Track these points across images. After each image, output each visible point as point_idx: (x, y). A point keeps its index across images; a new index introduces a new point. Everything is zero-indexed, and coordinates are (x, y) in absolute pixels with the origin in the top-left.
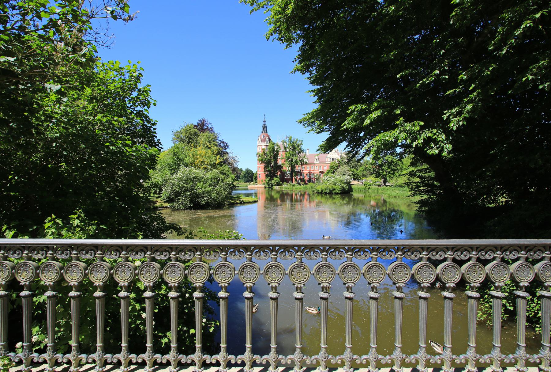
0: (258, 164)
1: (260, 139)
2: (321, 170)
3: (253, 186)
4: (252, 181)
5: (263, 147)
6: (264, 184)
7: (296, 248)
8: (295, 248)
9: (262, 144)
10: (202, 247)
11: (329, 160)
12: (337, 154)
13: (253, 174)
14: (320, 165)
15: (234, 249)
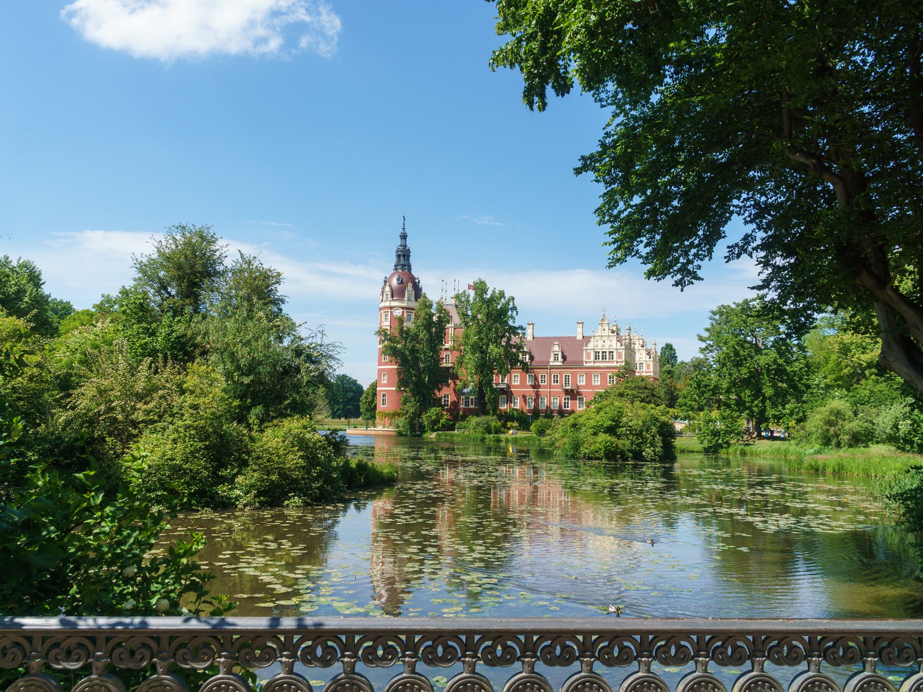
0: (380, 364)
1: (388, 289)
2: (569, 387)
3: (361, 430)
4: (357, 414)
5: (398, 313)
6: (398, 427)
7: (638, 637)
8: (401, 637)
9: (394, 304)
10: (235, 637)
11: (592, 358)
12: (615, 339)
13: (359, 390)
14: (568, 372)
15: (314, 640)
